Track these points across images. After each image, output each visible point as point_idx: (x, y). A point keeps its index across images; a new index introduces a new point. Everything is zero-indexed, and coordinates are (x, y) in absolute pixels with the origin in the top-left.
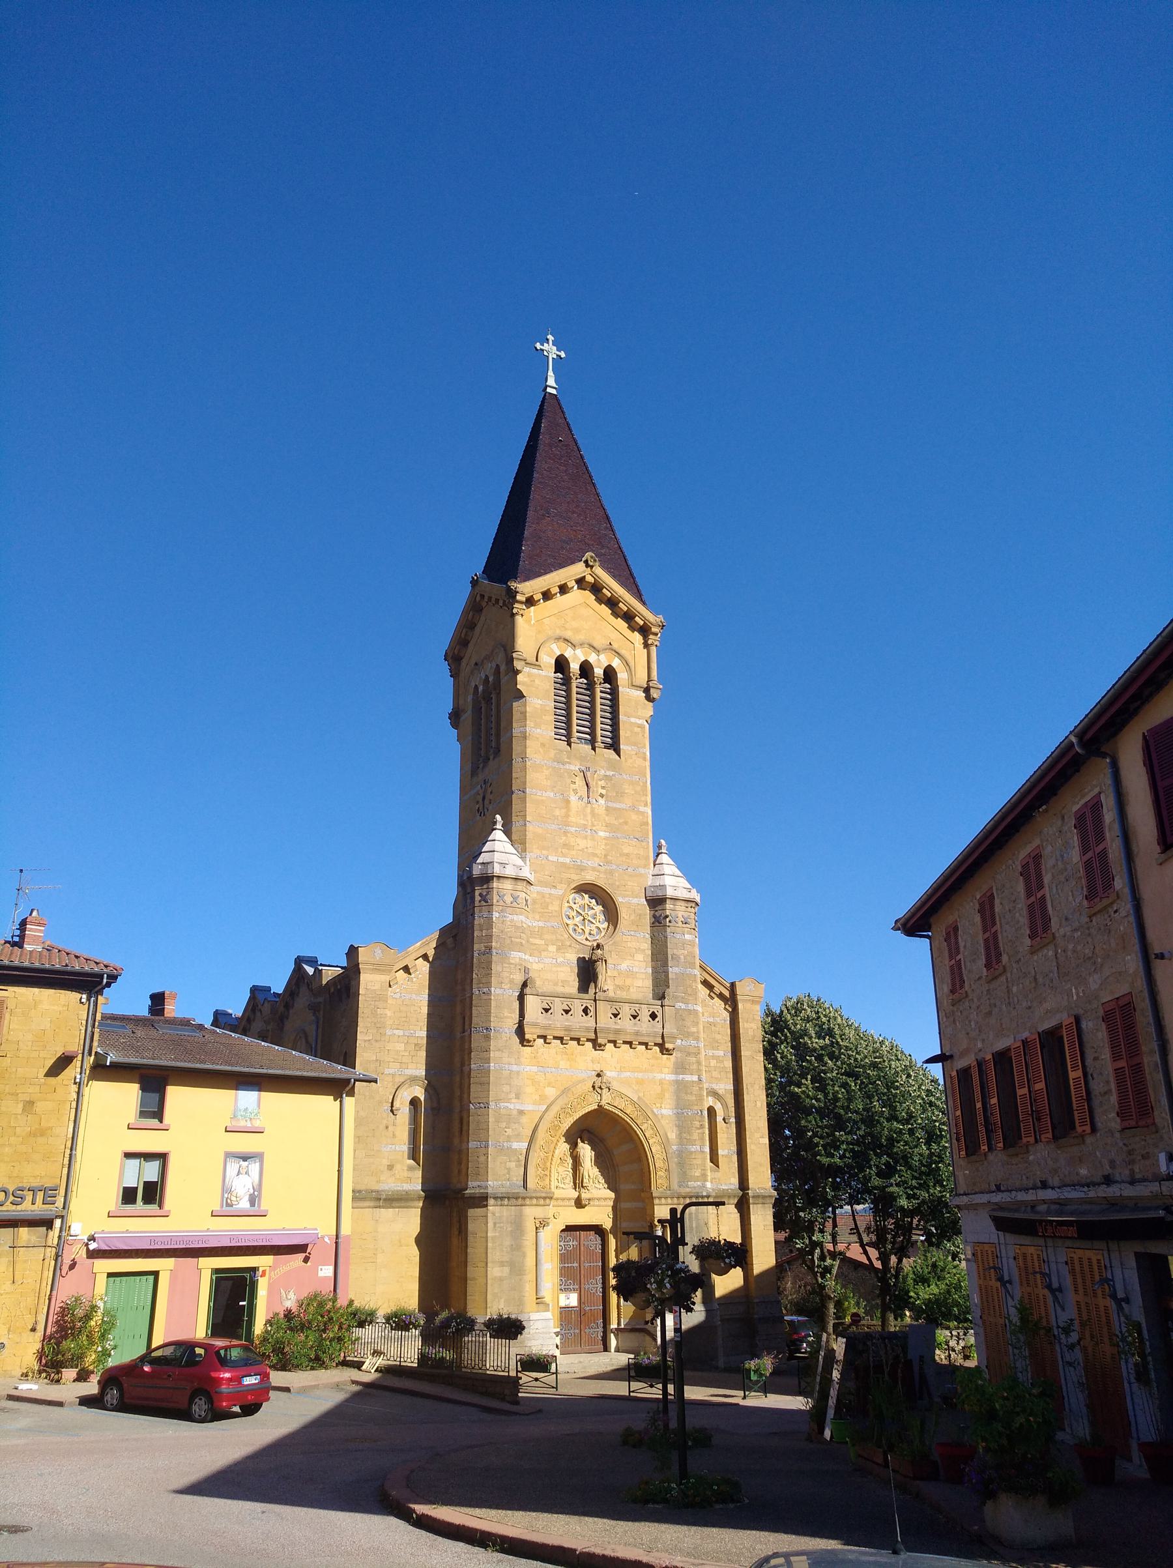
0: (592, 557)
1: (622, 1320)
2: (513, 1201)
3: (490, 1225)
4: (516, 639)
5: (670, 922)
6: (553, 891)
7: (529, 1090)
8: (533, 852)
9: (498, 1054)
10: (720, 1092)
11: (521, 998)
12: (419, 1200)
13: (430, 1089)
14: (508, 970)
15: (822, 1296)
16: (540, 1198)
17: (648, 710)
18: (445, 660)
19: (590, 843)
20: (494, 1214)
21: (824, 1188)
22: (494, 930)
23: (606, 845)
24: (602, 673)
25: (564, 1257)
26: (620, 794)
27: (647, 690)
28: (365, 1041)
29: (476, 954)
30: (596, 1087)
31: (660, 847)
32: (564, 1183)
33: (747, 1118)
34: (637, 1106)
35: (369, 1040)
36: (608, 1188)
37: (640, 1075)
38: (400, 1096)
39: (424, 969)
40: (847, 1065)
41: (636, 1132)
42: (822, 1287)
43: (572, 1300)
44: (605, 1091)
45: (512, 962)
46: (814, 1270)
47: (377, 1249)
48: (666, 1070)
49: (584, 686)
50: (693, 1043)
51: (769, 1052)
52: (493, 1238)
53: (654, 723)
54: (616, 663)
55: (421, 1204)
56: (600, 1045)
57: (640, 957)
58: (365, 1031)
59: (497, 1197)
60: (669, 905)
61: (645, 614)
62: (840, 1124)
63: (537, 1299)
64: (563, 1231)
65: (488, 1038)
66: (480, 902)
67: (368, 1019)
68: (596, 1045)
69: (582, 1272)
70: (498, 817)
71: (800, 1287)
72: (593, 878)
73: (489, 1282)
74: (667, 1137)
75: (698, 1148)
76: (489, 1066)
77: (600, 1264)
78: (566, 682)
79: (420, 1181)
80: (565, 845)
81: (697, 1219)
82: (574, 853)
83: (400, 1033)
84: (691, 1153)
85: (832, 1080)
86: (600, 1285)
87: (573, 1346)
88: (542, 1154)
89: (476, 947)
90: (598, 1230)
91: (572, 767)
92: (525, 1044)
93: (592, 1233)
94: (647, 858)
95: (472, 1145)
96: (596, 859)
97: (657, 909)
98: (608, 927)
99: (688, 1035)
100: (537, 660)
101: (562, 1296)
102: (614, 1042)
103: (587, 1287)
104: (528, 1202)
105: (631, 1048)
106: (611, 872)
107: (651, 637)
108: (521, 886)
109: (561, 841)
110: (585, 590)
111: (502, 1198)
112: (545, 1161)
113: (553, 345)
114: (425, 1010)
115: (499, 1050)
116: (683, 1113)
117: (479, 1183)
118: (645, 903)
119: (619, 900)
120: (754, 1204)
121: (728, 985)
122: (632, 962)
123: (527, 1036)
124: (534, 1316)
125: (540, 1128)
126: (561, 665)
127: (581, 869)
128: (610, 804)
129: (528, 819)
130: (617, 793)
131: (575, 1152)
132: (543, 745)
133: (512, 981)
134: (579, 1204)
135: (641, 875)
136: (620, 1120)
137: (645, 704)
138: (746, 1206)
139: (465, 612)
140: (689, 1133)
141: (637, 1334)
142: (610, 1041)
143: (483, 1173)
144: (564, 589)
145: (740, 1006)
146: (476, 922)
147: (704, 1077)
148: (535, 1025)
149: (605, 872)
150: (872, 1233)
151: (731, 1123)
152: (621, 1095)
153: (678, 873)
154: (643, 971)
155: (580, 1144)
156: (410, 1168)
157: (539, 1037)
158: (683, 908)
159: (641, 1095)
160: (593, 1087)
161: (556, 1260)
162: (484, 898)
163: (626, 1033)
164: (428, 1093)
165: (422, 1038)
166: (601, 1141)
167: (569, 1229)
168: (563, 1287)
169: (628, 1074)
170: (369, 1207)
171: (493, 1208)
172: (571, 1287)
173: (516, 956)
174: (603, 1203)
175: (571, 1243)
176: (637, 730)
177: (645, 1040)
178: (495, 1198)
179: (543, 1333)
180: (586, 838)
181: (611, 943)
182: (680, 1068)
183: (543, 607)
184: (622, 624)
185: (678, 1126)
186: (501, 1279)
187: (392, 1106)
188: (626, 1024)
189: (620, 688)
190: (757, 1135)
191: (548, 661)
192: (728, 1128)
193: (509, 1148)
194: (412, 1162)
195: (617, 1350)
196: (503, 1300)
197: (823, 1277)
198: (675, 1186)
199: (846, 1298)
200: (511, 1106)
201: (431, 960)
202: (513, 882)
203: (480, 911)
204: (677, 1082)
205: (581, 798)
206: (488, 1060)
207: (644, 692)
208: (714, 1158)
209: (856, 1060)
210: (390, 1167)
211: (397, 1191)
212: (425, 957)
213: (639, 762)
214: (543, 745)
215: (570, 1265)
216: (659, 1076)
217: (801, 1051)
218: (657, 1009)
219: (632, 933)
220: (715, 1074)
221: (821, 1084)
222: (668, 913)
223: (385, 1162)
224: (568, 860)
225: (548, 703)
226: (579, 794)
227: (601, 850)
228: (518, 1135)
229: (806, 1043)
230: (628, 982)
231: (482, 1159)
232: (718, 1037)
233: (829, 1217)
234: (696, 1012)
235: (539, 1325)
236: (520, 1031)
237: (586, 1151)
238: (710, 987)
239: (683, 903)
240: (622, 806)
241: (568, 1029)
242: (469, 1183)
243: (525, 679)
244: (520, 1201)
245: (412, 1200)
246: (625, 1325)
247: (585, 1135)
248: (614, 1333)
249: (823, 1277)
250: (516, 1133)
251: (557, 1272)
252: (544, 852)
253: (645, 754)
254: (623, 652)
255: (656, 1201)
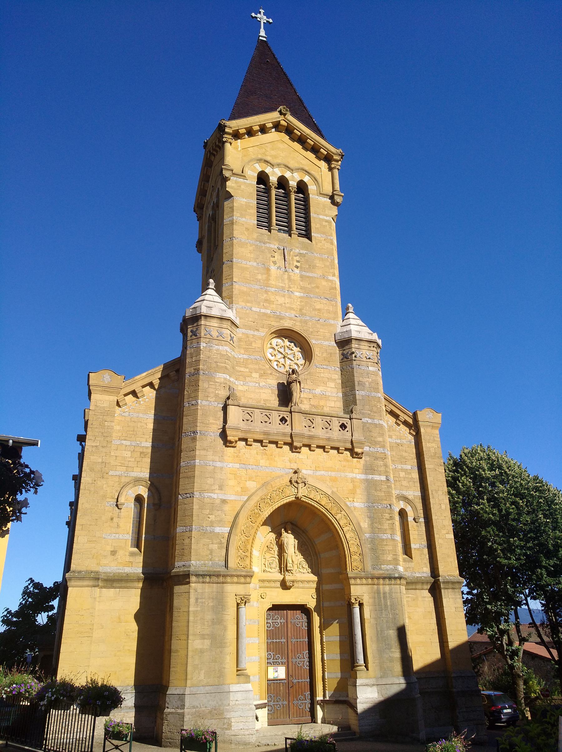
0: (284, 108)
1: (327, 692)
2: (214, 579)
3: (192, 600)
4: (225, 158)
5: (355, 357)
6: (256, 333)
7: (232, 483)
8: (239, 303)
9: (203, 453)
10: (410, 497)
11: (225, 409)
12: (139, 581)
13: (153, 487)
14: (214, 387)
15: (513, 674)
16: (241, 576)
17: (334, 211)
18: (194, 211)
19: (287, 300)
20: (196, 590)
21: (506, 586)
22: (202, 356)
23: (301, 302)
24: (296, 184)
25: (272, 634)
26: (312, 267)
27: (332, 198)
28: (93, 446)
29: (187, 376)
30: (293, 481)
31: (348, 308)
32: (271, 568)
33: (434, 517)
34: (331, 499)
35: (96, 446)
36: (312, 572)
37: (333, 474)
38: (124, 493)
39: (151, 395)
40: (515, 488)
41: (331, 521)
42: (512, 667)
43: (281, 673)
44: (301, 485)
45: (217, 381)
46: (504, 653)
47: (93, 624)
48: (357, 471)
49: (282, 195)
50: (381, 450)
51: (452, 483)
52: (195, 612)
53: (340, 221)
54: (306, 179)
55: (141, 585)
56: (296, 448)
57: (332, 385)
58: (93, 438)
59: (199, 575)
60: (354, 345)
61: (327, 146)
62: (513, 532)
63: (238, 671)
64: (269, 609)
65: (194, 439)
66: (191, 336)
67: (97, 430)
68: (293, 448)
69: (290, 647)
70: (211, 281)
71: (494, 670)
72: (290, 325)
73: (190, 654)
74: (360, 527)
75: (389, 536)
76: (195, 462)
77: (307, 640)
78: (267, 191)
79: (141, 565)
80: (266, 300)
81: (391, 598)
82: (274, 306)
83: (128, 443)
84: (383, 540)
85: (503, 499)
86: (307, 659)
87: (282, 717)
88: (243, 538)
89: (188, 370)
90: (303, 609)
91: (272, 246)
92: (228, 444)
93: (299, 612)
94: (336, 313)
95: (179, 530)
96: (292, 311)
97: (345, 348)
98: (305, 363)
99: (374, 443)
100: (242, 172)
101: (271, 669)
102: (309, 446)
103: (294, 660)
104: (229, 579)
105: (324, 451)
106: (306, 322)
107: (333, 162)
108: (226, 324)
109: (263, 297)
110: (281, 132)
111: (203, 576)
112: (245, 543)
113: (264, 15)
114: (151, 426)
115: (204, 449)
116: (374, 507)
117: (183, 563)
118: (335, 345)
119: (313, 342)
120: (445, 589)
121: (411, 414)
122: (326, 388)
123: (229, 438)
124: (234, 688)
125: (241, 515)
126: (262, 178)
127: (280, 318)
128: (304, 273)
129: (234, 280)
130: (309, 266)
131: (280, 541)
132: (247, 229)
133: (217, 396)
134: (284, 585)
135: (331, 325)
136: (317, 511)
137: (331, 207)
138: (438, 591)
139: (203, 169)
140: (380, 523)
141: (341, 706)
142: (305, 445)
143: (187, 553)
144: (263, 130)
145: (422, 430)
146: (188, 352)
147: (391, 478)
148: (237, 429)
149: (301, 321)
150: (547, 627)
151: (420, 522)
152: (317, 489)
153: (361, 323)
154: (334, 395)
155: (284, 534)
156: (132, 554)
157: (240, 439)
158: (367, 348)
159: (335, 490)
160: (290, 481)
161: (263, 635)
162: (194, 333)
163: (319, 438)
164: (151, 492)
165: (147, 448)
166: (303, 532)
167: (276, 608)
168: (271, 661)
169: (323, 472)
170: (88, 586)
171: (195, 586)
172: (280, 661)
173: (221, 377)
174: (307, 585)
175: (278, 621)
176: (324, 223)
177: (336, 445)
178: (197, 575)
179: (244, 704)
180: (284, 296)
181: (306, 373)
182: (369, 469)
183: (247, 141)
184: (310, 155)
185: (370, 517)
186: (202, 651)
187: (117, 501)
188: (319, 432)
189: (311, 196)
190: (444, 532)
191: (252, 175)
192: (417, 526)
193: (212, 532)
194: (136, 550)
195: (324, 721)
196: (203, 671)
197: (512, 659)
198: (369, 568)
199: (530, 679)
200: (215, 496)
201: (156, 387)
202: (218, 321)
203: (191, 343)
204: (367, 480)
205: (279, 268)
206: (194, 458)
207: (330, 199)
208: (407, 551)
209: (521, 484)
210: (113, 553)
211: (119, 573)
212: (151, 385)
213: (328, 245)
214: (247, 229)
215: (278, 641)
216: (351, 475)
217: (477, 479)
218: (346, 421)
219: (325, 367)
220: (405, 483)
221: (494, 501)
222: (353, 350)
223: (109, 548)
224: (268, 312)
225: (252, 201)
226: (278, 265)
227: (297, 305)
228: (220, 521)
229: (481, 474)
230: (322, 403)
231: (187, 541)
232: (405, 454)
233: (512, 609)
234: (381, 426)
235: (239, 696)
236: (223, 435)
237: (289, 540)
238: (396, 416)
239: (366, 344)
240: (315, 275)
241: (266, 433)
242: (176, 563)
243: (233, 185)
244: (221, 579)
245: (132, 581)
246: (329, 697)
247: (289, 526)
248: (320, 704)
249: (512, 659)
250: (219, 519)
251: (264, 647)
252: (248, 304)
253: (332, 240)
254: (312, 172)
255: (352, 581)
